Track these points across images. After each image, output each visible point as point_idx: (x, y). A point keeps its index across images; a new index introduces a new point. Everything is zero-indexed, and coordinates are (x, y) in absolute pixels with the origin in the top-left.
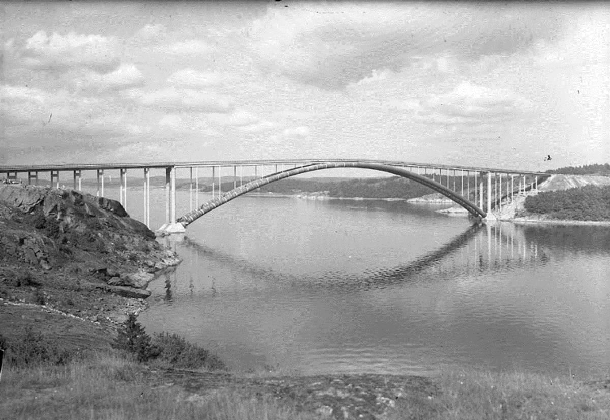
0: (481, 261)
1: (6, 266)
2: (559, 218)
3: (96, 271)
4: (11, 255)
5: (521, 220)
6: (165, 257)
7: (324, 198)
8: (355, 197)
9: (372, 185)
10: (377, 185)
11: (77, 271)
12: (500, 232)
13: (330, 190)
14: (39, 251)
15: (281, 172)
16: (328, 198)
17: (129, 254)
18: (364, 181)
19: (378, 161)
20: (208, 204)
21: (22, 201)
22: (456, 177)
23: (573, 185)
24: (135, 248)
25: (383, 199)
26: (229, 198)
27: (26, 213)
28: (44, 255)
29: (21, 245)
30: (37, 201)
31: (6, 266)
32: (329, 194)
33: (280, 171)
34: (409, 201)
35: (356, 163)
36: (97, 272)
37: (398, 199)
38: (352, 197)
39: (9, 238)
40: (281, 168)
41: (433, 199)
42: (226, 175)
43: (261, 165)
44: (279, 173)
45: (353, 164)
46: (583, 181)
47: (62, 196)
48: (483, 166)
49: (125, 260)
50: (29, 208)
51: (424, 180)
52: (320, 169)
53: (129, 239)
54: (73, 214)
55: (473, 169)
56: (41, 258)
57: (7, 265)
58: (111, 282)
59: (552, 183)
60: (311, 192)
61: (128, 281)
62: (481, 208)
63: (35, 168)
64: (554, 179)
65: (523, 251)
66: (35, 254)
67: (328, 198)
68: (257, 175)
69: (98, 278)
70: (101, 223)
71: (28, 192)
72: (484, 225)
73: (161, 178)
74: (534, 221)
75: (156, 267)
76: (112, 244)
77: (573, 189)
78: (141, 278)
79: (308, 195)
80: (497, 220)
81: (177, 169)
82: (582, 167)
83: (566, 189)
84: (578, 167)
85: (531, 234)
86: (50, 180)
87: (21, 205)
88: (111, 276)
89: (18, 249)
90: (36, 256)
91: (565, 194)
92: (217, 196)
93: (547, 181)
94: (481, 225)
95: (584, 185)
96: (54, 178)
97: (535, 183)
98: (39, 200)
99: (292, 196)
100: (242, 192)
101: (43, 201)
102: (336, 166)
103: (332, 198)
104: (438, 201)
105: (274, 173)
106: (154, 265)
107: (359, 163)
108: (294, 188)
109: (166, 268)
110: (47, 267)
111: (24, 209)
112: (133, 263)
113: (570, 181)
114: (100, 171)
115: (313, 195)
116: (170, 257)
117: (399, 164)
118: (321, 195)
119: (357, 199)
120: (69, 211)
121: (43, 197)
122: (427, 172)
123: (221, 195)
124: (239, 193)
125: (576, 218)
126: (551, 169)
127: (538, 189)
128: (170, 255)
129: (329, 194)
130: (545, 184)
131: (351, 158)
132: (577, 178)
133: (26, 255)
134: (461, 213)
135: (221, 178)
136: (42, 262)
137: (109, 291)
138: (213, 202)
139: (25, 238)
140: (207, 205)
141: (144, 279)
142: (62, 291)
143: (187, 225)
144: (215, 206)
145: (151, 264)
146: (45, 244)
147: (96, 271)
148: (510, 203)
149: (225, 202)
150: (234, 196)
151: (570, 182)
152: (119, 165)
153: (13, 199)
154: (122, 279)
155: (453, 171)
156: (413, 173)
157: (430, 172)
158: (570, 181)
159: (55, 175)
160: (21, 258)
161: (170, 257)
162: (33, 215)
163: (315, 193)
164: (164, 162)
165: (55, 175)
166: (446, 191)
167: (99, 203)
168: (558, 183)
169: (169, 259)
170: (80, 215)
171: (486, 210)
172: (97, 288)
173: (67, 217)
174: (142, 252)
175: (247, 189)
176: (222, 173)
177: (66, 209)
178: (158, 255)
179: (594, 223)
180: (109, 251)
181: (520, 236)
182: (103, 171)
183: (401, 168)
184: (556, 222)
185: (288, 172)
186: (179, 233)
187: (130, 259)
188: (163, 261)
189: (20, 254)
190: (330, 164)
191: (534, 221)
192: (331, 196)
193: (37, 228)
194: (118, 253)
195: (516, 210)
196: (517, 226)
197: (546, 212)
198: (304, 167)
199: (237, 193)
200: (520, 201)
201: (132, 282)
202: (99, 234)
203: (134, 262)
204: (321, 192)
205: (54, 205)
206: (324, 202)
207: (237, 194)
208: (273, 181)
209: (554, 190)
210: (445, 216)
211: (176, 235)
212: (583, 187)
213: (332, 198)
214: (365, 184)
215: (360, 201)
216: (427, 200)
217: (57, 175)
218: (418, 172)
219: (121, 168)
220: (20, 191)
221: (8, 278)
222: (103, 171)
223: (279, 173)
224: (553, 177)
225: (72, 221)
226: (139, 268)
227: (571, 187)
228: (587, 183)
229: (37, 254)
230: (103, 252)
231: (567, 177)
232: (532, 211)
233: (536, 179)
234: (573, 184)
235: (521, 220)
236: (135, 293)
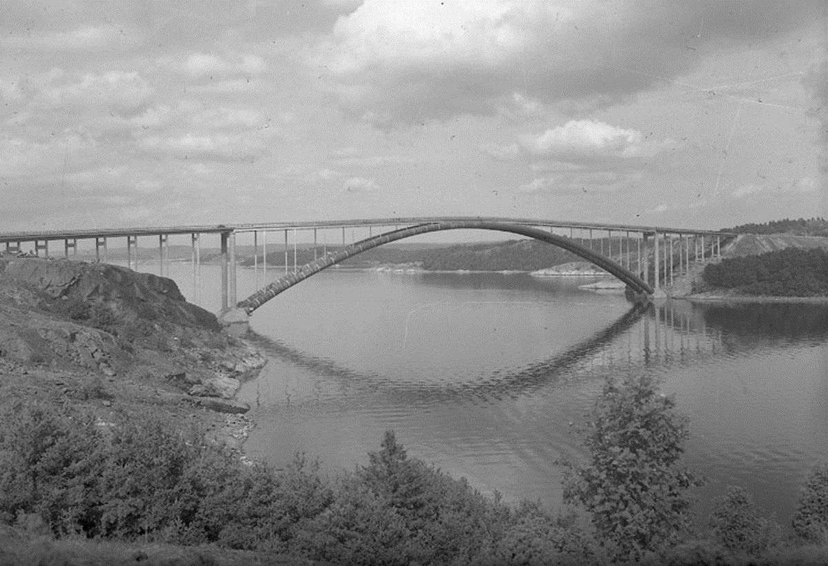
1: (59, 372)
2: (752, 293)
3: (173, 376)
4: (61, 356)
5: (701, 297)
6: (246, 356)
7: (415, 272)
8: (458, 269)
9: (481, 253)
10: (487, 252)
11: (148, 376)
13: (422, 261)
14: (97, 350)
15: (379, 236)
16: (421, 271)
17: (201, 352)
18: (469, 248)
20: (279, 281)
21: (51, 281)
22: (594, 240)
23: (768, 248)
24: (206, 344)
25: (496, 272)
27: (55, 299)
28: (104, 355)
29: (73, 342)
30: (71, 281)
31: (59, 372)
32: (422, 266)
34: (533, 273)
36: (175, 378)
37: (518, 272)
38: (454, 270)
39: (56, 332)
40: (378, 231)
41: (567, 271)
43: (262, 231)
46: (781, 243)
47: (104, 273)
48: (648, 225)
49: (195, 361)
50: (60, 291)
52: (430, 230)
53: (195, 332)
54: (119, 298)
55: (635, 230)
56: (101, 359)
57: (61, 371)
58: (194, 391)
59: (739, 246)
60: (396, 263)
61: (214, 391)
62: (646, 282)
64: (742, 240)
66: (92, 354)
67: (421, 271)
68: (318, 242)
69: (176, 386)
70: (156, 310)
72: (650, 305)
75: (237, 369)
76: (176, 338)
77: (769, 254)
78: (227, 386)
79: (392, 267)
80: (668, 297)
81: (237, 234)
82: (768, 224)
83: (759, 254)
84: (763, 223)
85: (716, 318)
86: (191, 245)
87: (48, 286)
88: (191, 384)
89: (70, 349)
90: (93, 357)
93: (732, 244)
95: (783, 248)
96: (100, 247)
97: (717, 246)
98: (74, 278)
99: (371, 269)
100: (326, 265)
101: (79, 280)
102: (452, 226)
103: (426, 272)
104: (574, 273)
105: (368, 237)
106: (235, 367)
107: (483, 222)
108: (369, 259)
109: (250, 371)
110: (109, 372)
111: (53, 292)
112: (207, 366)
113: (764, 242)
114: (132, 238)
115: (400, 268)
116: (252, 356)
117: (536, 223)
118: (411, 267)
119: (461, 272)
120: (114, 293)
121: (79, 274)
122: (612, 235)
123: (297, 268)
124: (323, 265)
126: (725, 227)
128: (253, 353)
129: (422, 266)
130: (729, 247)
131: (505, 217)
132: (773, 238)
133: (81, 355)
134: (613, 288)
136: (103, 365)
137: (199, 403)
138: (286, 279)
139: (77, 333)
140: (278, 283)
141: (231, 386)
142: (141, 405)
143: (251, 311)
144: (289, 285)
145: (231, 365)
146: (103, 340)
147: (173, 376)
148: (684, 274)
149: (303, 279)
150: (316, 270)
151: (764, 245)
152: (189, 228)
153: (38, 278)
154: (207, 387)
155: (589, 231)
156: (555, 235)
158: (764, 242)
159: (102, 244)
160: (75, 360)
161: (252, 356)
162: (66, 300)
163: (402, 265)
164: (214, 224)
165: (102, 244)
166: (600, 259)
167: (149, 283)
169: (251, 358)
170: (128, 299)
172: (184, 400)
173: (111, 301)
174: (217, 350)
176: (299, 238)
177: (111, 290)
178: (238, 354)
180: (172, 349)
182: (166, 236)
184: (749, 299)
185: (387, 236)
186: (240, 323)
187: (203, 359)
188: (244, 362)
189: (73, 354)
192: (425, 269)
193: (74, 318)
194: (186, 351)
195: (693, 284)
196: (695, 305)
197: (734, 286)
199: (320, 265)
200: (699, 271)
201: (218, 392)
202: (156, 326)
203: (208, 363)
204: (411, 264)
205: (94, 285)
206: (415, 277)
207: (319, 268)
208: (368, 248)
209: (744, 256)
210: (592, 294)
211: (238, 326)
212: (782, 251)
213: (426, 272)
214: (471, 251)
216: (558, 271)
217: (73, 245)
218: (558, 232)
219: (193, 232)
220: (47, 267)
221: (70, 388)
222: (166, 236)
223: (374, 238)
224: (740, 237)
225: (118, 308)
226: (216, 371)
227: (766, 251)
228: (787, 245)
229: (95, 355)
230: (167, 351)
235: (701, 297)
236: (231, 406)
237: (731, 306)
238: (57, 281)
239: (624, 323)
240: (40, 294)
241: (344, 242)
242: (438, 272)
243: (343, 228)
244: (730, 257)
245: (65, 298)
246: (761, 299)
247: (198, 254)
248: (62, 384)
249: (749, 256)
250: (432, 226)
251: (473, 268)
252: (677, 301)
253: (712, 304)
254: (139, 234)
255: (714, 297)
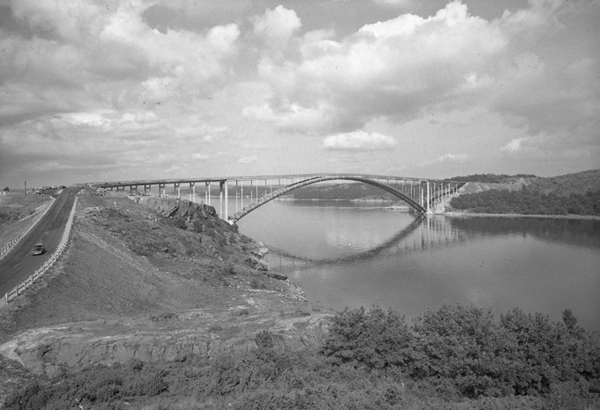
0: (423, 241)
5: (451, 214)
9: (323, 190)
10: (326, 190)
12: (435, 223)
15: (297, 183)
16: (293, 199)
19: (359, 175)
26: (263, 202)
27: (167, 218)
32: (294, 197)
33: (295, 182)
34: (351, 201)
35: (345, 177)
42: (274, 184)
44: (294, 184)
45: (343, 177)
51: (387, 187)
63: (193, 180)
65: (449, 234)
67: (293, 199)
71: (167, 202)
72: (425, 217)
73: (172, 188)
74: (458, 214)
85: (456, 223)
87: (163, 211)
91: (477, 195)
92: (254, 202)
93: (463, 188)
94: (422, 217)
98: (175, 207)
101: (178, 208)
103: (296, 200)
105: (291, 183)
115: (283, 198)
116: (262, 247)
118: (288, 197)
121: (178, 205)
125: (488, 212)
127: (458, 192)
129: (294, 197)
135: (258, 187)
153: (157, 207)
157: (390, 181)
158: (479, 187)
165: (162, 187)
168: (471, 188)
171: (426, 205)
175: (275, 195)
177: (194, 213)
179: (501, 215)
181: (448, 226)
183: (373, 179)
184: (474, 215)
190: (328, 177)
191: (458, 214)
192: (296, 198)
196: (446, 217)
197: (466, 208)
198: (312, 179)
200: (448, 200)
205: (186, 211)
206: (291, 202)
209: (470, 193)
213: (296, 200)
215: (316, 201)
218: (381, 181)
223: (294, 184)
231: (476, 184)
232: (457, 208)
233: (456, 185)
234: (480, 188)
235: (451, 214)
237: (465, 218)
238: (168, 209)
239: (412, 227)
240: (159, 216)
241: (266, 183)
242: (302, 200)
243: (292, 179)
244: (463, 194)
245: (171, 217)
246: (481, 215)
247: (209, 191)
248: (213, 267)
249: (472, 194)
250: (323, 178)
251: (320, 198)
252: (438, 216)
253: (456, 217)
254: (181, 182)
255: (457, 214)
